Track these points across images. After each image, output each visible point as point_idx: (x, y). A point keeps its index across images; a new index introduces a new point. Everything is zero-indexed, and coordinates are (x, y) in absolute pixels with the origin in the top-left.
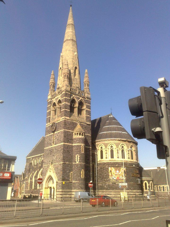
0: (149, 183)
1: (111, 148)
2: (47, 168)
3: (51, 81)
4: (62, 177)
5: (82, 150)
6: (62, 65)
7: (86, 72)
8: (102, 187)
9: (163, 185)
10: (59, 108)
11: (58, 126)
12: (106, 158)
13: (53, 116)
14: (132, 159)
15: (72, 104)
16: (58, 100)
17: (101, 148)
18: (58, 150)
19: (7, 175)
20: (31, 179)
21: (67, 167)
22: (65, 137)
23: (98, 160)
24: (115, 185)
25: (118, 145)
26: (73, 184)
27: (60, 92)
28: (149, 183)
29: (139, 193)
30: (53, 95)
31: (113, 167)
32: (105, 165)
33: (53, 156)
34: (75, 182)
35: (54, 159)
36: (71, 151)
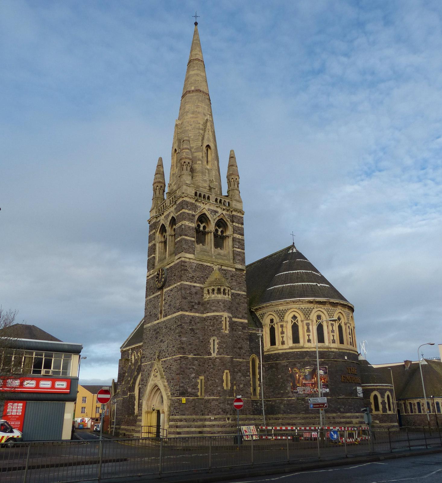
0: (383, 397)
1: (293, 320)
5: (223, 327)
10: (172, 236)
14: (342, 342)
15: (203, 228)
16: (170, 218)
17: (272, 321)
19: (61, 385)
23: (265, 349)
25: (308, 314)
26: (205, 402)
28: (384, 395)
29: (358, 419)
30: (160, 208)
33: (161, 341)
34: (209, 398)
35: (164, 348)
36: (199, 329)
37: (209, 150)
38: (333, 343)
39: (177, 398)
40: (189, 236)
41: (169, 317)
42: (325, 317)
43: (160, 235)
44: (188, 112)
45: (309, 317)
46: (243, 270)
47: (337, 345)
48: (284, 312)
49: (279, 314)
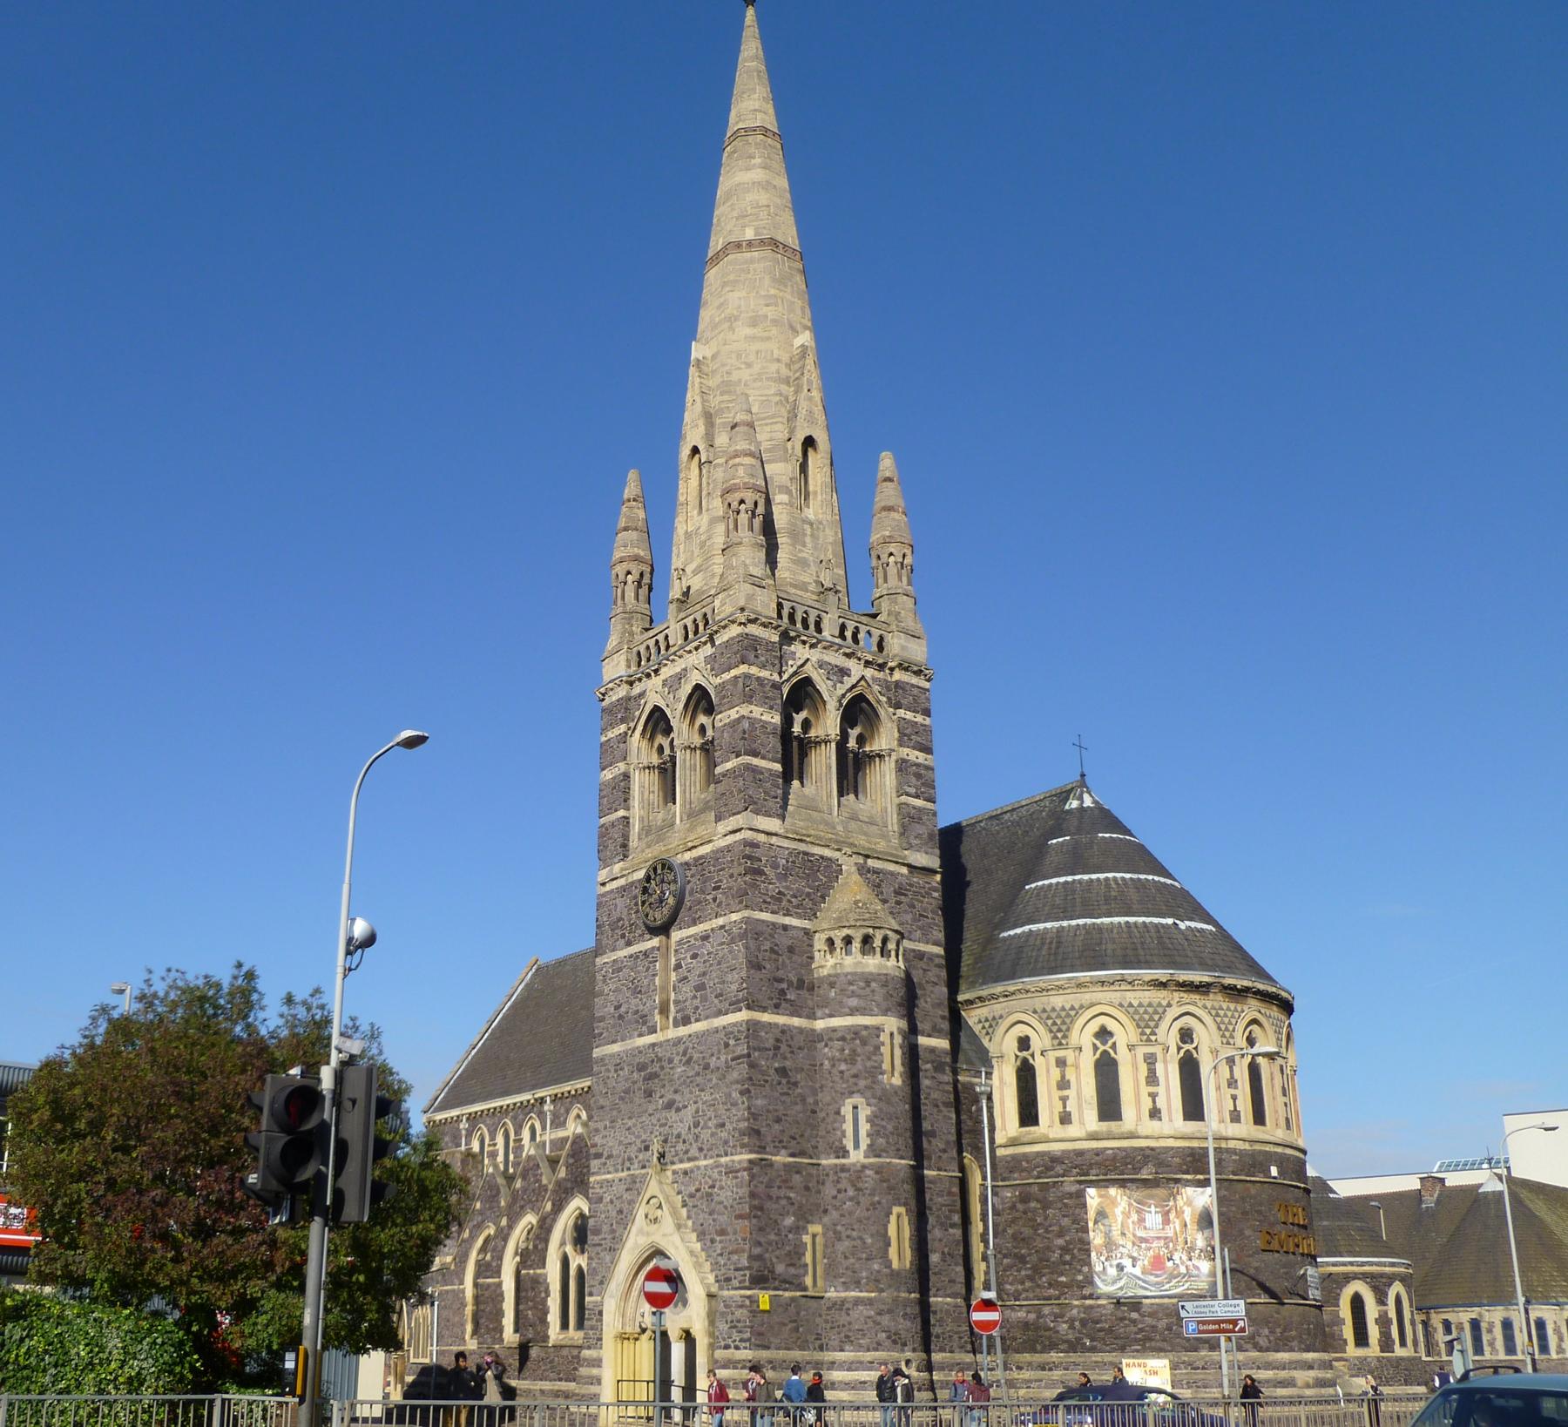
0: (1381, 1301)
1: (1098, 1043)
2: (626, 1196)
3: (627, 545)
4: (751, 1258)
6: (702, 429)
7: (888, 474)
8: (1037, 1328)
9: (1473, 1313)
11: (695, 883)
12: (1065, 1119)
13: (647, 806)
14: (1259, 1118)
16: (687, 689)
17: (1024, 1043)
18: (706, 1067)
20: (488, 1269)
21: (782, 1193)
22: (759, 967)
23: (999, 1139)
24: (1134, 1315)
25: (1152, 1024)
26: (829, 1309)
27: (696, 632)
29: (1312, 1373)
30: (642, 649)
31: (1122, 1184)
32: (1059, 1169)
33: (669, 1105)
34: (843, 1295)
35: (681, 1128)
37: (811, 452)
38: (1232, 1121)
39: (743, 1292)
40: (763, 758)
41: (696, 1027)
42: (1206, 1040)
43: (644, 743)
44: (736, 319)
45: (1153, 1033)
46: (934, 872)
47: (1246, 1128)
48: (1068, 1015)
49: (1050, 1022)
